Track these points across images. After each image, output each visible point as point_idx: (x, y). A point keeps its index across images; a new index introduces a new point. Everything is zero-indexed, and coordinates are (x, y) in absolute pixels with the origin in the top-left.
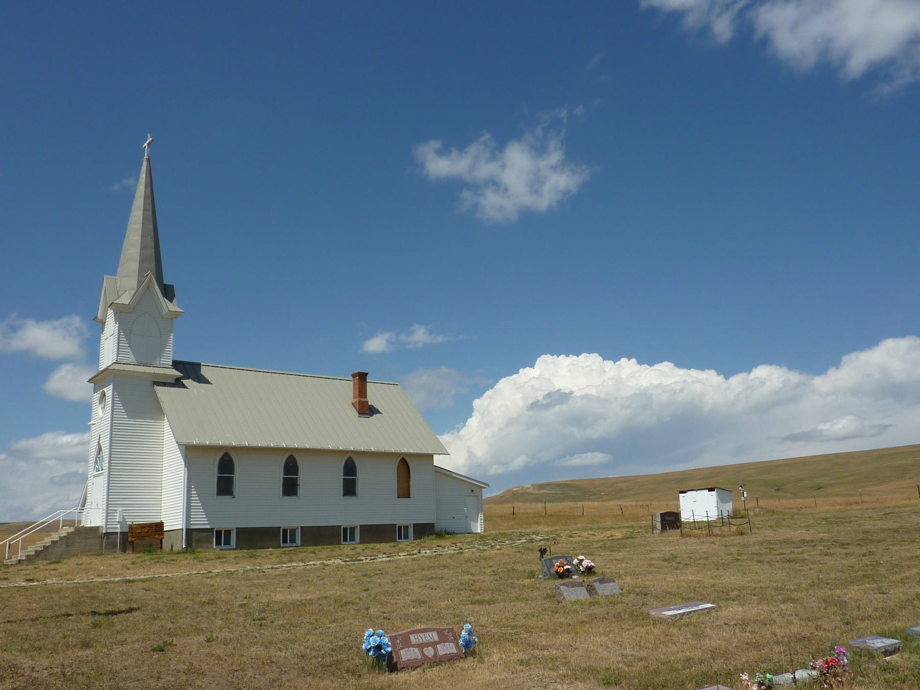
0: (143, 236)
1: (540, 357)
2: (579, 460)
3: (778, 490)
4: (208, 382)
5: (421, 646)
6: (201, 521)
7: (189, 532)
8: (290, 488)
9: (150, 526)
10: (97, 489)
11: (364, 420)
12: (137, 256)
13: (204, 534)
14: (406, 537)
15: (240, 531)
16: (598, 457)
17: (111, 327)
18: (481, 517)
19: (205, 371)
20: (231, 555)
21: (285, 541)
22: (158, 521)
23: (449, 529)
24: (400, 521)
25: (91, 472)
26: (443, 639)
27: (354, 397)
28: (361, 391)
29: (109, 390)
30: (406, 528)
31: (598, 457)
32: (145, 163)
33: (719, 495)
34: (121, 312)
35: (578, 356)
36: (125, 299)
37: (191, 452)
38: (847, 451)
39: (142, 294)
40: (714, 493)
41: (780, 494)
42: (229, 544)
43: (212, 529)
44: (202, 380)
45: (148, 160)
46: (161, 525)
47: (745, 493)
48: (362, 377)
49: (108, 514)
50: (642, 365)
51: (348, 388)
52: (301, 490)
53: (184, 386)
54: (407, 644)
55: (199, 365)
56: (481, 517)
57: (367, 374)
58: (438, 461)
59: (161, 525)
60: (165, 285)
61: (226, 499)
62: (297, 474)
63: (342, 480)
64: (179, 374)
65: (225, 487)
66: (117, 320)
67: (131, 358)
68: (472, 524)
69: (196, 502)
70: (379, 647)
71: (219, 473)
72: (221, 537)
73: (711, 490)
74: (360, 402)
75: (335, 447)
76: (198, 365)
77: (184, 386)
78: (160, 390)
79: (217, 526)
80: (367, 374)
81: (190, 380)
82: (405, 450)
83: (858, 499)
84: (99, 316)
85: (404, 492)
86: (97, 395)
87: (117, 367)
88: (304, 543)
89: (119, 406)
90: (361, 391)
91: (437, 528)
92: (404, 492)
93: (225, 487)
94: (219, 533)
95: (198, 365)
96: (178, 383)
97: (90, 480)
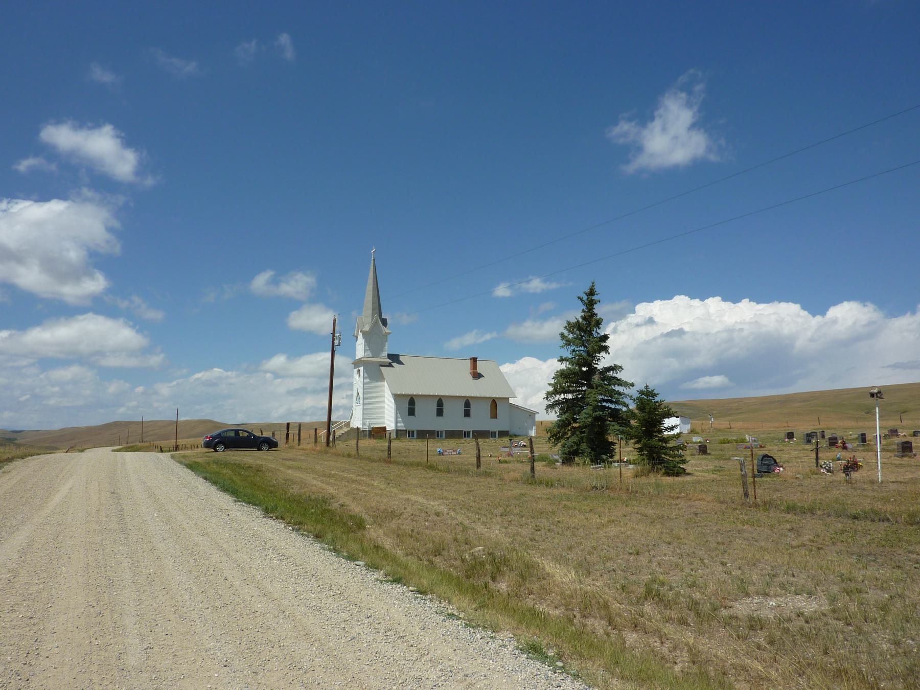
0: (373, 297)
1: (651, 301)
2: (706, 382)
3: (867, 413)
4: (403, 364)
5: (449, 452)
6: (402, 427)
7: (397, 431)
8: (440, 413)
9: (381, 428)
10: (358, 412)
11: (476, 381)
12: (371, 307)
13: (403, 432)
14: (469, 437)
15: (418, 431)
16: (717, 380)
17: (361, 340)
18: (534, 428)
19: (401, 358)
20: (415, 441)
21: (438, 436)
22: (383, 426)
23: (517, 434)
24: (437, 428)
25: (355, 404)
26: (454, 451)
27: (471, 370)
28: (474, 366)
29: (361, 369)
30: (495, 433)
31: (717, 380)
32: (372, 261)
33: (680, 419)
34: (365, 334)
35: (691, 299)
36: (367, 328)
37: (397, 397)
38: (908, 383)
39: (374, 326)
40: (678, 419)
41: (869, 415)
42: (414, 436)
43: (406, 430)
44: (400, 363)
45: (374, 260)
46: (385, 428)
47: (712, 419)
48: (474, 360)
49: (364, 422)
50: (752, 302)
51: (469, 364)
52: (445, 414)
53: (393, 367)
54: (446, 452)
55: (399, 355)
56: (534, 428)
57: (477, 358)
58: (511, 401)
59: (385, 428)
60: (383, 319)
61: (412, 417)
62: (442, 407)
63: (471, 407)
64: (390, 361)
65: (411, 412)
66: (364, 337)
67: (370, 355)
68: (530, 431)
69: (399, 419)
70: (440, 451)
71: (409, 406)
72: (410, 434)
73: (677, 417)
74: (473, 372)
75: (460, 395)
76: (398, 356)
77: (393, 367)
78: (382, 368)
79: (408, 429)
80: (477, 358)
81: (395, 363)
82: (494, 396)
83: (786, 425)
84: (355, 335)
85: (494, 415)
86: (356, 370)
87: (365, 359)
88: (447, 437)
89: (366, 376)
90: (474, 366)
91: (511, 433)
92: (494, 415)
93: (411, 412)
94: (409, 432)
95: (398, 356)
96: (390, 365)
97: (354, 408)
